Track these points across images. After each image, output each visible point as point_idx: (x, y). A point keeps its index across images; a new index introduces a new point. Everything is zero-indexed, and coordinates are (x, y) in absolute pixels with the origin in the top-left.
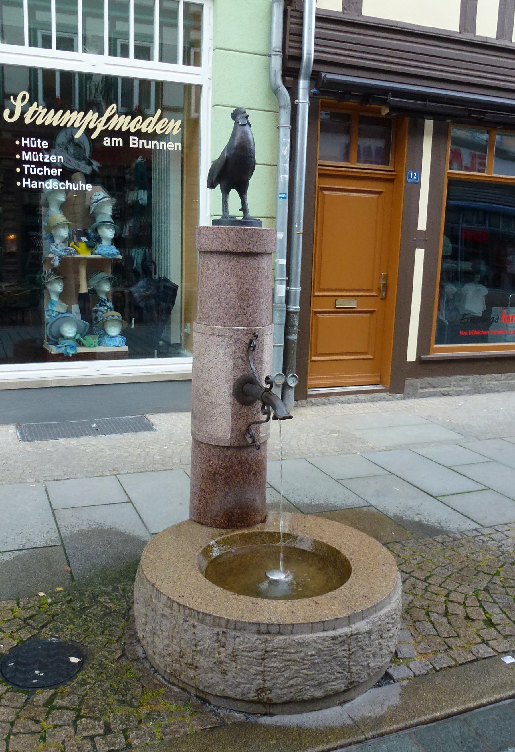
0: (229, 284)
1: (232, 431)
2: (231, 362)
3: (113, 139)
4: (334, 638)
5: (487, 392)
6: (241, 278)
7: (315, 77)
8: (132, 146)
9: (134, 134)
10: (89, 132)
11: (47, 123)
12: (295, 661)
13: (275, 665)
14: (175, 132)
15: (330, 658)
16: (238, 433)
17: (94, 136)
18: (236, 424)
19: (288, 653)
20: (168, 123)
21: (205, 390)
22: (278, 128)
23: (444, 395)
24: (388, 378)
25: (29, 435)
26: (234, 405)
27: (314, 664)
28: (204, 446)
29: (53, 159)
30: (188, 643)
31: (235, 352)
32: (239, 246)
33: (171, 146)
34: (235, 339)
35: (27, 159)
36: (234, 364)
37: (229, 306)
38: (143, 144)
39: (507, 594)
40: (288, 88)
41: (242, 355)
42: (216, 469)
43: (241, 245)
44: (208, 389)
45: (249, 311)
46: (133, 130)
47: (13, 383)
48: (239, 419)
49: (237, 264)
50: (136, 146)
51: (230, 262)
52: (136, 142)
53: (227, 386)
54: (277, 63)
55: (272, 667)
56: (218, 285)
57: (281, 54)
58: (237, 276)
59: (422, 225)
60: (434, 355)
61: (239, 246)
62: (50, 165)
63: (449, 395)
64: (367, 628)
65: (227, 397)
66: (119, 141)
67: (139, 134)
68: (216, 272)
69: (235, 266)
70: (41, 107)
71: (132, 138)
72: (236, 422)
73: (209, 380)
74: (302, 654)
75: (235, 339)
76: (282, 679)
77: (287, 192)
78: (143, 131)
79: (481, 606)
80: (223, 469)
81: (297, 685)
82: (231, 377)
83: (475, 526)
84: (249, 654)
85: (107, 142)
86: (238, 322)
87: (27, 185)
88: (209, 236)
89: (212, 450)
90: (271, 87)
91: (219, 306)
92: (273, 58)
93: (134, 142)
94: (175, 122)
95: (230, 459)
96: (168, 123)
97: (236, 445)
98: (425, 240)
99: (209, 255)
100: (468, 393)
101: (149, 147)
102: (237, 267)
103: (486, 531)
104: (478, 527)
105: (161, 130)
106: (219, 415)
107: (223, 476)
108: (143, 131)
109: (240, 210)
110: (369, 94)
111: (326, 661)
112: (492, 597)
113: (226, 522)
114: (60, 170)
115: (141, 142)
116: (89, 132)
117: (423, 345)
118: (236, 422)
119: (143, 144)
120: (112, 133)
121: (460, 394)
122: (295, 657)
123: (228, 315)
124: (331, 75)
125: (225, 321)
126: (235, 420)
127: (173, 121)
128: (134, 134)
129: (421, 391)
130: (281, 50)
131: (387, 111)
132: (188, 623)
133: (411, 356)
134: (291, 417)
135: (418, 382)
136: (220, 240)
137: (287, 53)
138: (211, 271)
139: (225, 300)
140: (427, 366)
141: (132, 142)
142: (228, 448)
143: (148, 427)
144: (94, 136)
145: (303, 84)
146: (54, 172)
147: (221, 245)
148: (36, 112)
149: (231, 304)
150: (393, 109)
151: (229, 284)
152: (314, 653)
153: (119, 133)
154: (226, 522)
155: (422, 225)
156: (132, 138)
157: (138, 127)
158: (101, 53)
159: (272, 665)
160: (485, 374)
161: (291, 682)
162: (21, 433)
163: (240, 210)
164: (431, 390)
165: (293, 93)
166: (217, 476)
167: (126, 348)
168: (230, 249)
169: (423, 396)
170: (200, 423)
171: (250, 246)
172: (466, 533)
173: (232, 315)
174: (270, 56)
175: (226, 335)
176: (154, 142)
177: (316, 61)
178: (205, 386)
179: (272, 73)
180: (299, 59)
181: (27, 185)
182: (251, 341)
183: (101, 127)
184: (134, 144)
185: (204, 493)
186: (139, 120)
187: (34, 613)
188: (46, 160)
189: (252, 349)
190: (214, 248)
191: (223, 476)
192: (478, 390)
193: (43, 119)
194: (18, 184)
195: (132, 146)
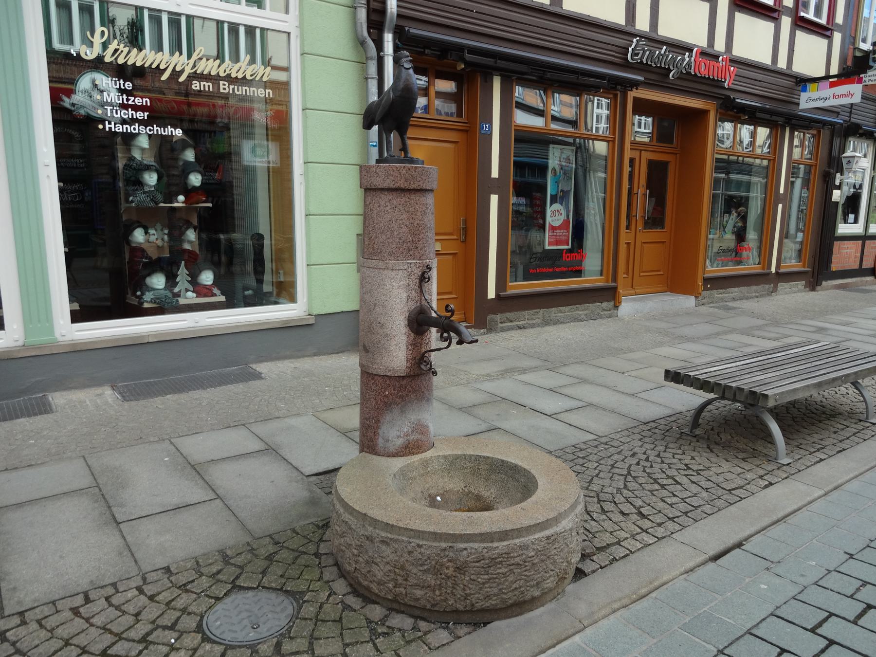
1: (408, 361)
2: (404, 295)
3: (202, 84)
4: (548, 538)
5: (554, 324)
7: (399, 33)
8: (222, 91)
9: (223, 79)
10: (176, 74)
11: (129, 63)
12: (518, 564)
13: (500, 571)
15: (545, 557)
17: (182, 79)
19: (511, 557)
22: (367, 79)
23: (520, 328)
24: (472, 314)
25: (130, 394)
27: (533, 564)
29: (138, 101)
30: (413, 564)
31: (409, 285)
35: (109, 100)
38: (233, 89)
39: (644, 489)
40: (373, 40)
44: (382, 322)
45: (420, 245)
46: (222, 74)
47: (104, 341)
50: (226, 91)
52: (226, 87)
53: (403, 317)
54: (362, 14)
55: (498, 573)
58: (408, 212)
59: (495, 173)
60: (510, 292)
62: (136, 108)
63: (524, 328)
64: (570, 525)
66: (207, 86)
67: (228, 78)
68: (387, 208)
70: (122, 45)
71: (221, 83)
74: (524, 556)
76: (507, 583)
77: (377, 140)
78: (233, 76)
79: (628, 502)
81: (520, 587)
82: (406, 309)
83: (592, 437)
84: (477, 564)
85: (196, 86)
87: (110, 128)
88: (380, 174)
89: (388, 382)
90: (358, 39)
92: (359, 10)
93: (225, 87)
97: (411, 373)
98: (497, 186)
99: (379, 193)
100: (539, 325)
101: (240, 93)
104: (596, 437)
108: (233, 76)
109: (401, 150)
110: (445, 49)
111: (543, 561)
114: (146, 114)
115: (231, 87)
116: (176, 74)
117: (501, 284)
119: (233, 89)
120: (201, 77)
121: (533, 326)
122: (517, 560)
128: (223, 79)
129: (501, 325)
131: (463, 66)
133: (491, 294)
134: (477, 341)
135: (498, 317)
138: (382, 208)
140: (508, 302)
141: (222, 87)
142: (403, 377)
143: (44, 408)
144: (182, 79)
145: (388, 38)
146: (140, 115)
148: (116, 50)
150: (467, 64)
152: (533, 554)
153: (207, 77)
155: (495, 173)
156: (221, 83)
157: (228, 72)
159: (499, 571)
160: (524, 310)
161: (514, 586)
162: (120, 393)
163: (401, 150)
164: (509, 324)
165: (380, 46)
167: (222, 298)
168: (402, 186)
169: (503, 330)
171: (421, 183)
174: (355, 8)
176: (244, 88)
177: (399, 16)
179: (359, 25)
180: (383, 12)
181: (110, 128)
182: (423, 273)
183: (188, 71)
184: (224, 89)
187: (220, 568)
188: (130, 102)
190: (385, 185)
192: (547, 323)
194: (101, 127)
195: (222, 91)
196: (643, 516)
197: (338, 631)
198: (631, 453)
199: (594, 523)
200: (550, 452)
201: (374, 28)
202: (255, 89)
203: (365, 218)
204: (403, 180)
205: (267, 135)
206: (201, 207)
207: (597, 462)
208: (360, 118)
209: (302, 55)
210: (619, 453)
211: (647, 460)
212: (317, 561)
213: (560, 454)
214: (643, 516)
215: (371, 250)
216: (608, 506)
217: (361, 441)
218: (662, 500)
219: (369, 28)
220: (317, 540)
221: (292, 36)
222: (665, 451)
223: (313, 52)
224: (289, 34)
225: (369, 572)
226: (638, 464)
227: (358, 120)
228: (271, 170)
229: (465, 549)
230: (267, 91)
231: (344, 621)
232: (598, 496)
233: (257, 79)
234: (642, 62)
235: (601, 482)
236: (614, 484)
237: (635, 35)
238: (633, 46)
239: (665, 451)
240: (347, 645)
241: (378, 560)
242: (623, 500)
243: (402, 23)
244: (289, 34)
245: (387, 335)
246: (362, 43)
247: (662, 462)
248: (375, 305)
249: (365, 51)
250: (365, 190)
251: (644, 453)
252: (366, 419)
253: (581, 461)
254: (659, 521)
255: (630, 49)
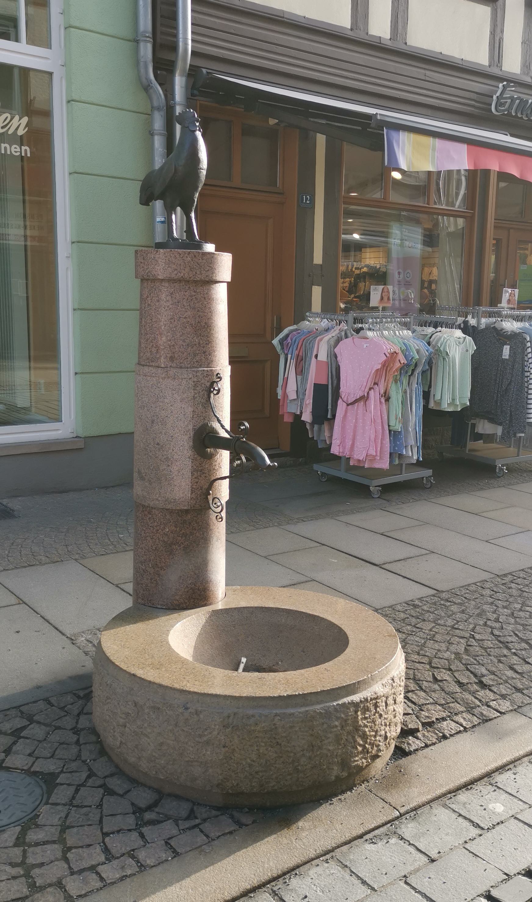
0: (185, 318)
6: (198, 311)
14: (21, 132)
16: (199, 493)
18: (197, 482)
20: (10, 121)
21: (158, 444)
26: (194, 460)
28: (157, 512)
31: (194, 398)
32: (196, 273)
33: (16, 150)
34: (194, 382)
36: (193, 411)
37: (186, 344)
39: (489, 655)
41: (202, 401)
42: (174, 538)
43: (198, 272)
48: (200, 476)
49: (194, 294)
51: (186, 292)
53: (186, 438)
54: (146, 50)
56: (171, 319)
57: (151, 40)
58: (194, 308)
61: (196, 273)
65: (185, 452)
69: (191, 296)
72: (197, 480)
73: (164, 431)
74: (325, 726)
75: (194, 382)
79: (468, 669)
80: (182, 537)
82: (191, 427)
86: (197, 362)
89: (168, 517)
90: (141, 83)
91: (173, 343)
92: (142, 45)
94: (20, 120)
95: (190, 523)
96: (10, 121)
102: (194, 297)
103: (444, 595)
105: (2, 128)
106: (176, 473)
107: (182, 546)
112: (486, 652)
113: (186, 601)
118: (197, 480)
123: (186, 353)
124: (206, 66)
125: (181, 361)
126: (196, 478)
127: (17, 117)
130: (151, 36)
132: (189, 711)
136: (174, 266)
137: (158, 40)
139: (181, 336)
142: (187, 511)
145: (179, 83)
147: (176, 272)
149: (187, 341)
151: (185, 318)
154: (186, 601)
158: (17, 40)
166: (174, 547)
170: (150, 484)
172: (424, 599)
173: (189, 354)
175: (183, 377)
177: (194, 53)
178: (157, 440)
180: (174, 48)
185: (157, 569)
186: (7, 118)
189: (215, 392)
191: (182, 546)
193: (4, 122)
196: (483, 685)
197: (98, 817)
198: (478, 611)
199: (422, 694)
200: (376, 610)
201: (161, 69)
202: (7, 146)
203: (141, 314)
204: (187, 270)
205: (24, 202)
206: (195, 140)
207: (434, 622)
208: (138, 186)
209: (69, 102)
210: (463, 612)
211: (497, 620)
212: (75, 738)
213: (387, 612)
214: (483, 685)
215: (148, 355)
216: (444, 675)
217: (135, 590)
218: (512, 668)
219: (155, 69)
220: (76, 712)
221: (55, 78)
222: (521, 610)
223: (83, 99)
224: (51, 74)
225: (136, 746)
226: (485, 624)
227: (134, 191)
228: (29, 248)
229: (253, 716)
230: (23, 148)
231: (105, 806)
232: (430, 663)
233: (10, 132)
234: (509, 114)
235: (436, 646)
236: (453, 648)
237: (500, 79)
238: (498, 94)
239: (521, 610)
240: (106, 834)
241: (149, 731)
242: (462, 667)
243: (199, 62)
244: (51, 74)
245: (167, 459)
246: (147, 88)
247: (516, 623)
248: (153, 422)
249: (150, 98)
250: (142, 280)
251: (494, 612)
252: (141, 563)
253: (414, 621)
254: (504, 692)
255: (495, 97)
